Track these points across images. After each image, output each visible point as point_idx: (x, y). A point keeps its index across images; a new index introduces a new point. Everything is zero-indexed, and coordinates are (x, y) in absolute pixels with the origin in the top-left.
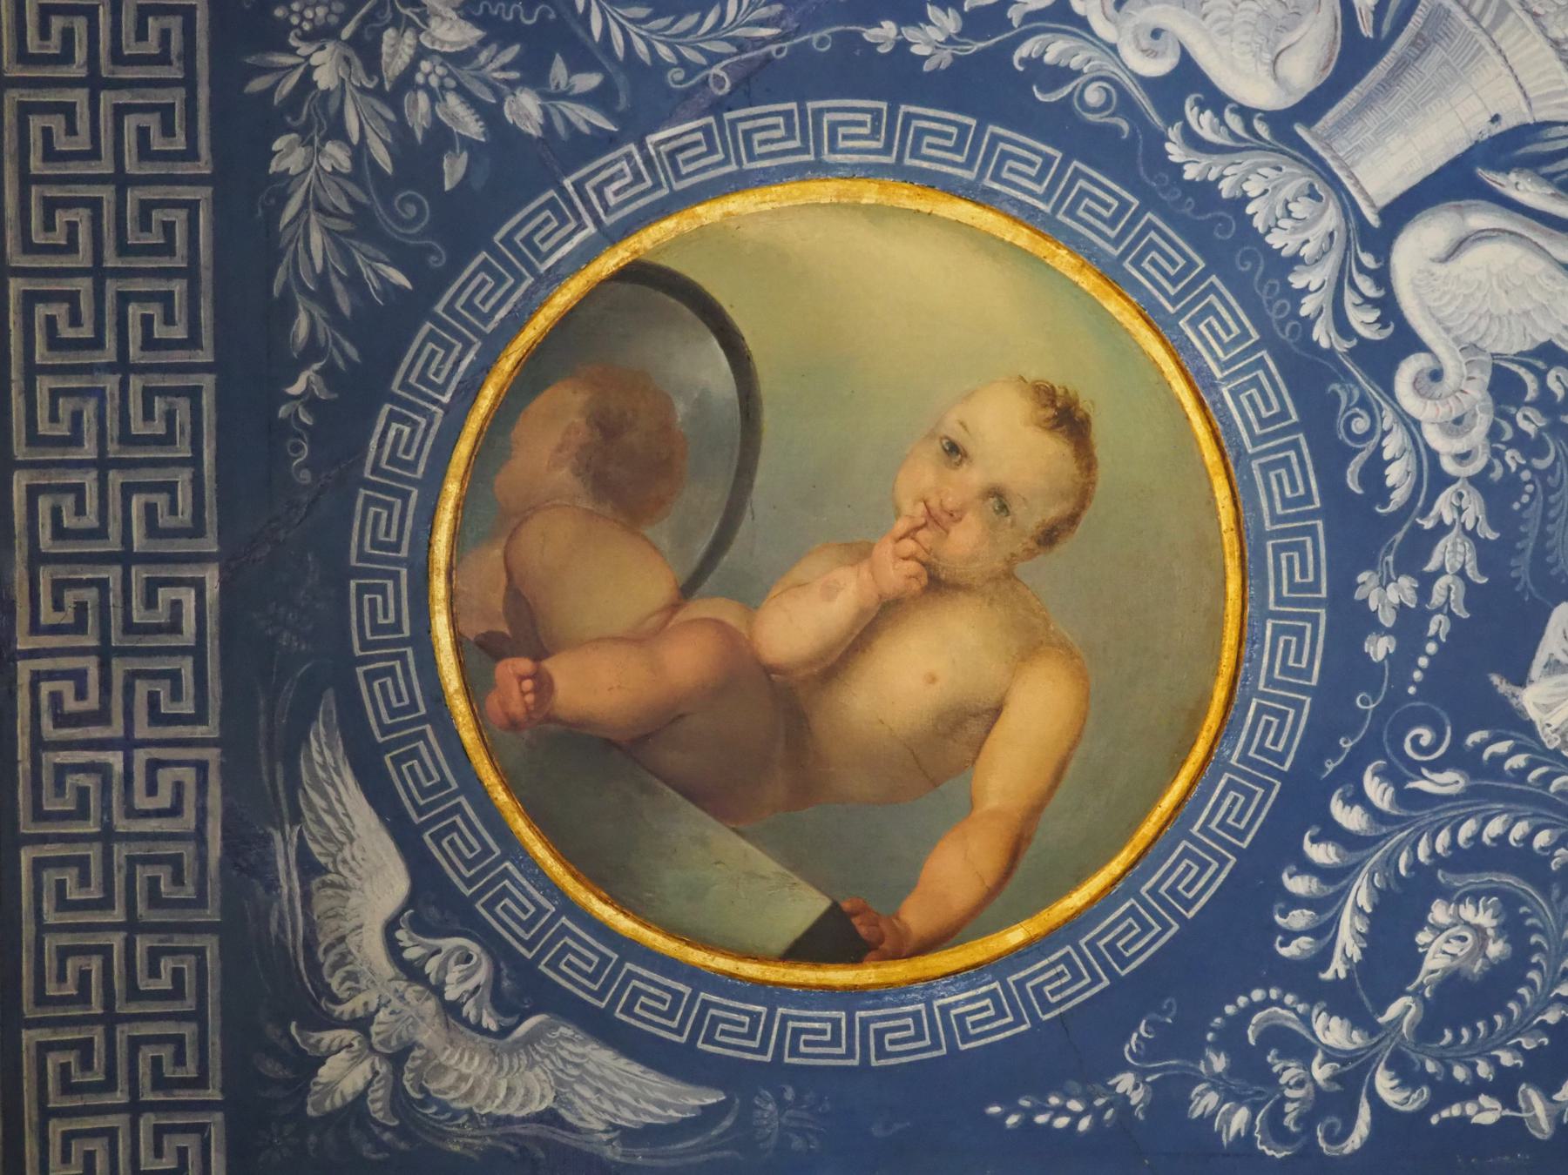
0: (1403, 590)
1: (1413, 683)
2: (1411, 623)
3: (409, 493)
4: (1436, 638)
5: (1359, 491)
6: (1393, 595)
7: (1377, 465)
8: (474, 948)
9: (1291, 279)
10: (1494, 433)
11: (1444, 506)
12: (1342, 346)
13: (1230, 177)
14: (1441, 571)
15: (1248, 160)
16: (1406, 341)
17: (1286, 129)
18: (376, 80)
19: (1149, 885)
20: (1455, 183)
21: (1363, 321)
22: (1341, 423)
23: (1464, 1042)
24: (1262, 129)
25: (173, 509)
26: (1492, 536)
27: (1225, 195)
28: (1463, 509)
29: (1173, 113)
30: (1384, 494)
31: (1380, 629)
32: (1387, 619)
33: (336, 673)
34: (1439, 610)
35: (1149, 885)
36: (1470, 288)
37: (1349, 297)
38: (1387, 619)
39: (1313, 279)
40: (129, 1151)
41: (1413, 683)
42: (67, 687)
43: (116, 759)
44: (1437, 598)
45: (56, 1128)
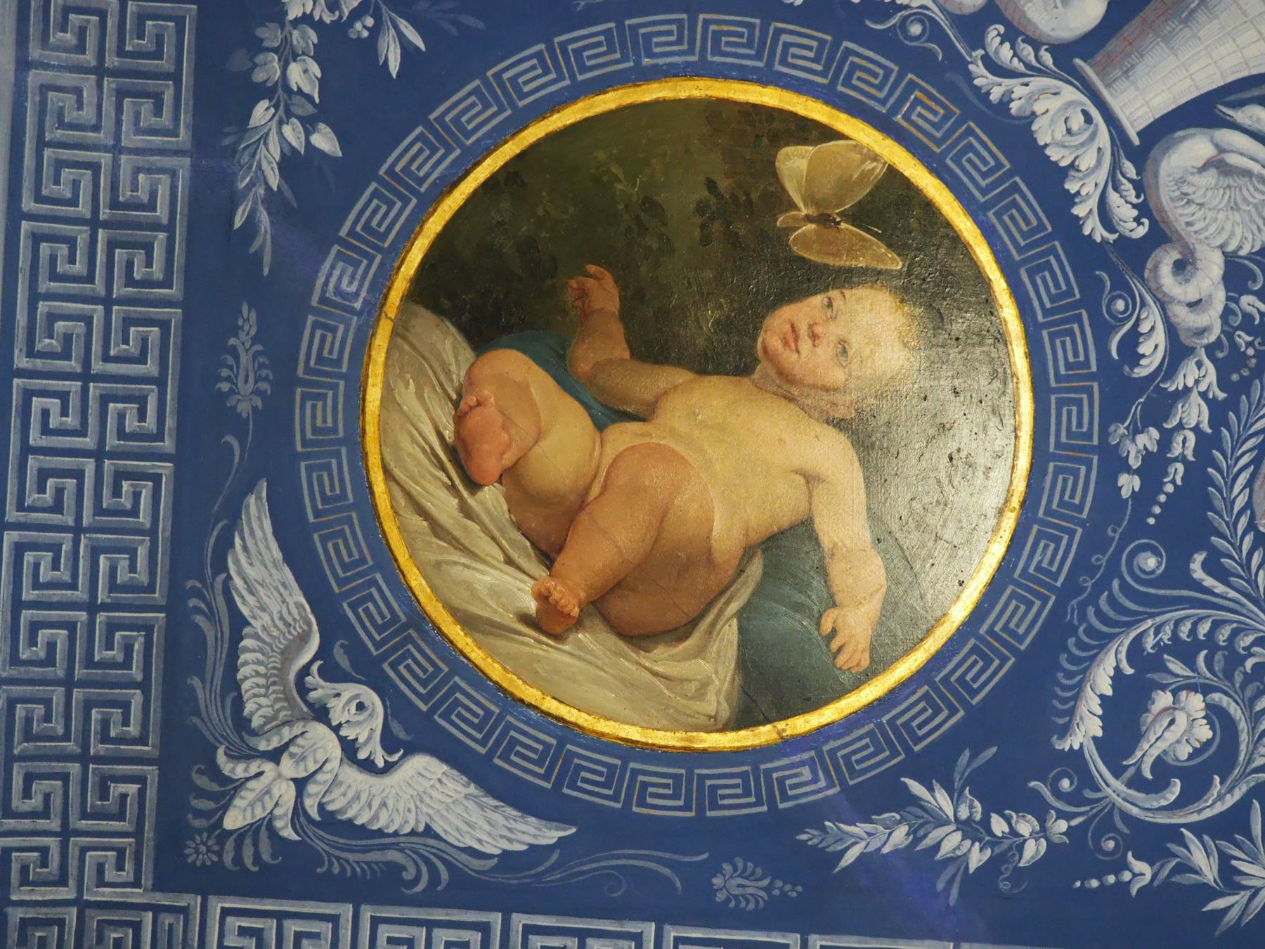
0: (1149, 439)
1: (1160, 505)
2: (1154, 466)
3: (337, 385)
4: (1173, 482)
5: (1116, 357)
6: (1142, 440)
7: (1133, 338)
8: (372, 698)
9: (1067, 186)
10: (1226, 314)
11: (1188, 374)
12: (1112, 237)
13: (1021, 95)
14: (1180, 426)
15: (1038, 82)
16: (1160, 235)
17: (1070, 58)
18: (337, 13)
19: (977, 194)
20: (1202, 112)
21: (1124, 211)
22: (1104, 303)
23: (1205, 652)
24: (1047, 58)
25: (133, 568)
26: (1221, 396)
27: (1013, 111)
28: (1199, 375)
29: (977, 41)
30: (1136, 359)
31: (1128, 470)
32: (1135, 462)
33: (274, 458)
34: (1176, 460)
35: (977, 194)
36: (1212, 204)
37: (1113, 197)
38: (1135, 462)
39: (1086, 189)
40: (85, 645)
41: (1160, 505)
42: (54, 404)
43: (105, 159)
44: (1177, 450)
45: (33, 462)
